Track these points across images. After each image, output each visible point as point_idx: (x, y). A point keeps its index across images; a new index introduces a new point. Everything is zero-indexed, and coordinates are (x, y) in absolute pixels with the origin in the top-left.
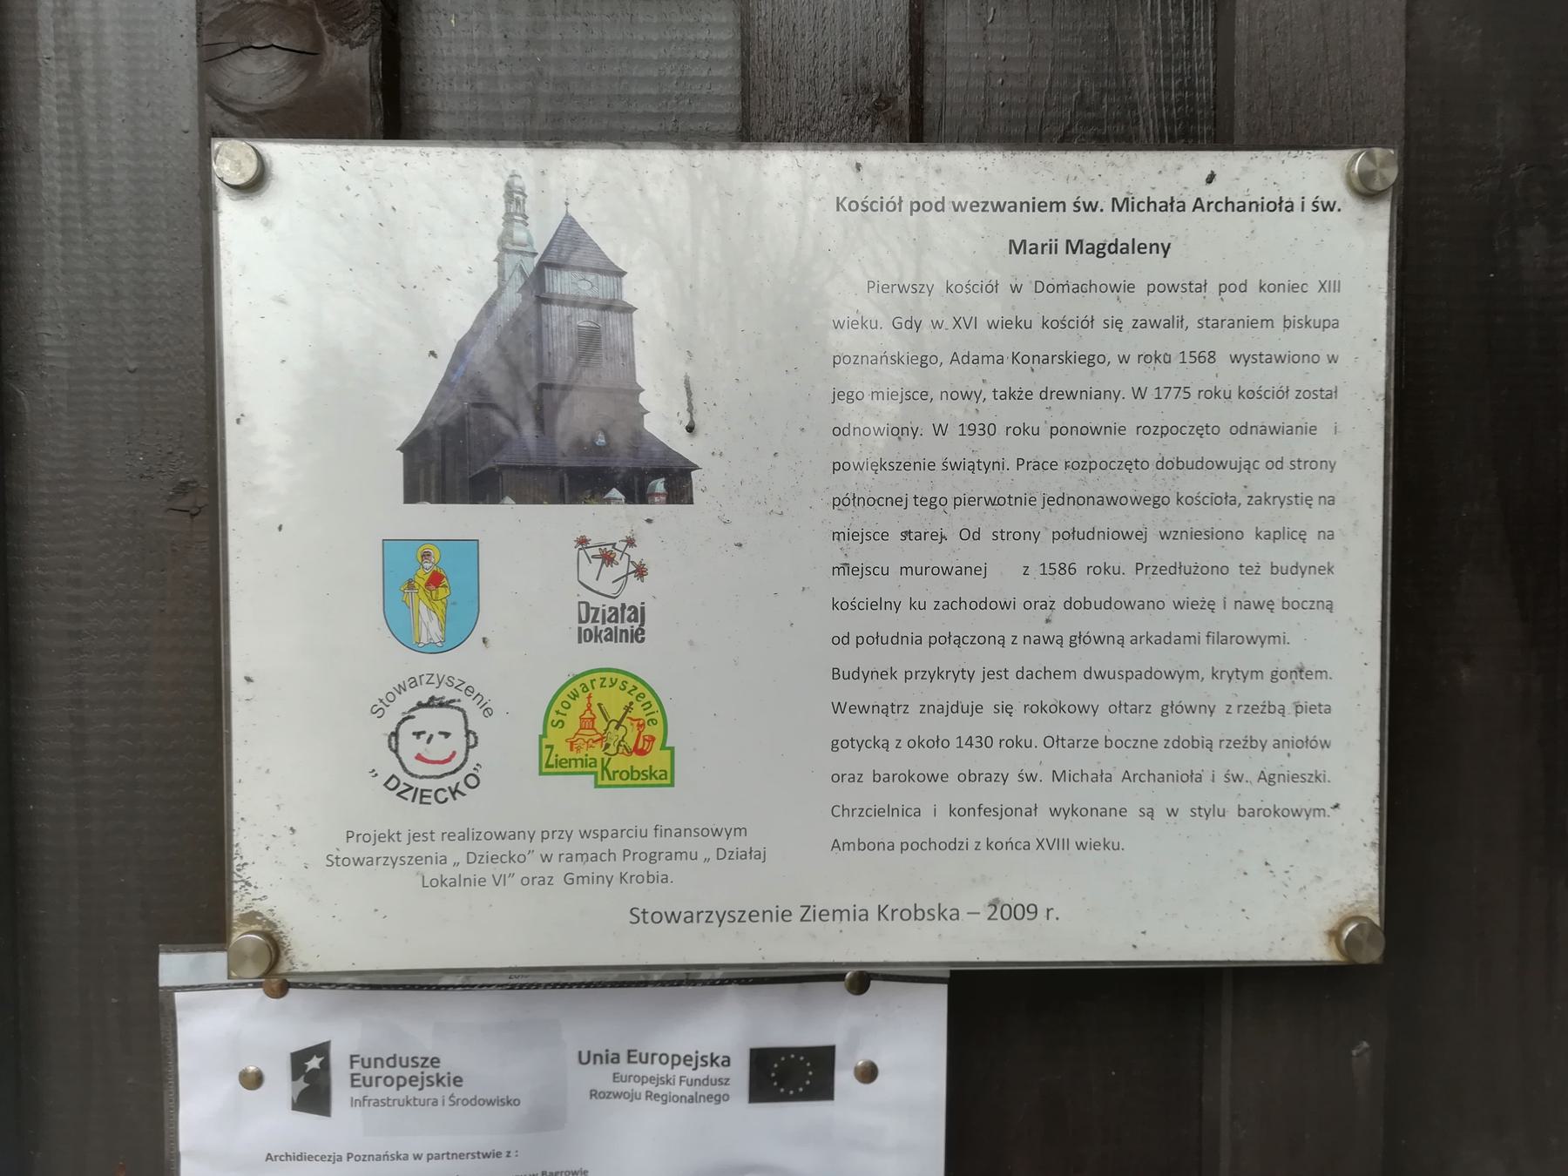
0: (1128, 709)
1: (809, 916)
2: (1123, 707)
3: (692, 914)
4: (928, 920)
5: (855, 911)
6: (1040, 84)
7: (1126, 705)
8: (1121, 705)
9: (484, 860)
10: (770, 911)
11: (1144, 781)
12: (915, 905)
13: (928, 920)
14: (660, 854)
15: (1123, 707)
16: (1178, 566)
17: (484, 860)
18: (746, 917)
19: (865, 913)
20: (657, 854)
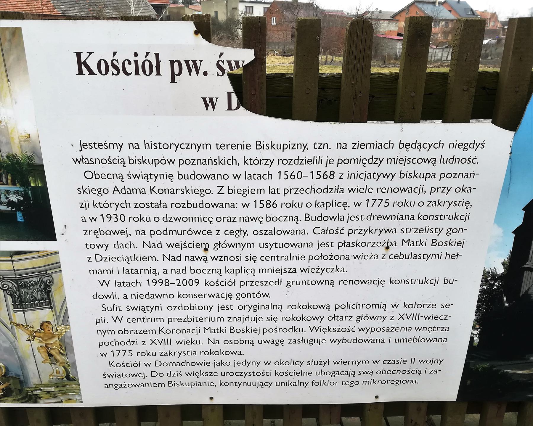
0: (339, 318)
1: (356, 146)
2: (336, 318)
3: (147, 175)
4: (467, 163)
5: (377, 144)
6: (477, 342)
7: (337, 317)
8: (335, 317)
9: (108, 259)
10: (278, 149)
11: (162, 149)
12: (400, 140)
13: (467, 163)
14: (292, 282)
15: (336, 318)
16: (280, 281)
17: (108, 259)
18: (268, 283)
19: (343, 217)
20: (291, 282)
